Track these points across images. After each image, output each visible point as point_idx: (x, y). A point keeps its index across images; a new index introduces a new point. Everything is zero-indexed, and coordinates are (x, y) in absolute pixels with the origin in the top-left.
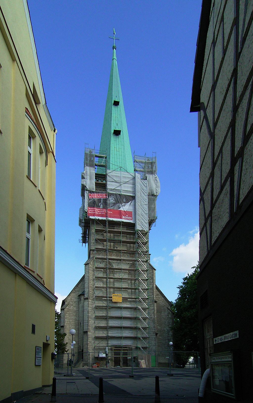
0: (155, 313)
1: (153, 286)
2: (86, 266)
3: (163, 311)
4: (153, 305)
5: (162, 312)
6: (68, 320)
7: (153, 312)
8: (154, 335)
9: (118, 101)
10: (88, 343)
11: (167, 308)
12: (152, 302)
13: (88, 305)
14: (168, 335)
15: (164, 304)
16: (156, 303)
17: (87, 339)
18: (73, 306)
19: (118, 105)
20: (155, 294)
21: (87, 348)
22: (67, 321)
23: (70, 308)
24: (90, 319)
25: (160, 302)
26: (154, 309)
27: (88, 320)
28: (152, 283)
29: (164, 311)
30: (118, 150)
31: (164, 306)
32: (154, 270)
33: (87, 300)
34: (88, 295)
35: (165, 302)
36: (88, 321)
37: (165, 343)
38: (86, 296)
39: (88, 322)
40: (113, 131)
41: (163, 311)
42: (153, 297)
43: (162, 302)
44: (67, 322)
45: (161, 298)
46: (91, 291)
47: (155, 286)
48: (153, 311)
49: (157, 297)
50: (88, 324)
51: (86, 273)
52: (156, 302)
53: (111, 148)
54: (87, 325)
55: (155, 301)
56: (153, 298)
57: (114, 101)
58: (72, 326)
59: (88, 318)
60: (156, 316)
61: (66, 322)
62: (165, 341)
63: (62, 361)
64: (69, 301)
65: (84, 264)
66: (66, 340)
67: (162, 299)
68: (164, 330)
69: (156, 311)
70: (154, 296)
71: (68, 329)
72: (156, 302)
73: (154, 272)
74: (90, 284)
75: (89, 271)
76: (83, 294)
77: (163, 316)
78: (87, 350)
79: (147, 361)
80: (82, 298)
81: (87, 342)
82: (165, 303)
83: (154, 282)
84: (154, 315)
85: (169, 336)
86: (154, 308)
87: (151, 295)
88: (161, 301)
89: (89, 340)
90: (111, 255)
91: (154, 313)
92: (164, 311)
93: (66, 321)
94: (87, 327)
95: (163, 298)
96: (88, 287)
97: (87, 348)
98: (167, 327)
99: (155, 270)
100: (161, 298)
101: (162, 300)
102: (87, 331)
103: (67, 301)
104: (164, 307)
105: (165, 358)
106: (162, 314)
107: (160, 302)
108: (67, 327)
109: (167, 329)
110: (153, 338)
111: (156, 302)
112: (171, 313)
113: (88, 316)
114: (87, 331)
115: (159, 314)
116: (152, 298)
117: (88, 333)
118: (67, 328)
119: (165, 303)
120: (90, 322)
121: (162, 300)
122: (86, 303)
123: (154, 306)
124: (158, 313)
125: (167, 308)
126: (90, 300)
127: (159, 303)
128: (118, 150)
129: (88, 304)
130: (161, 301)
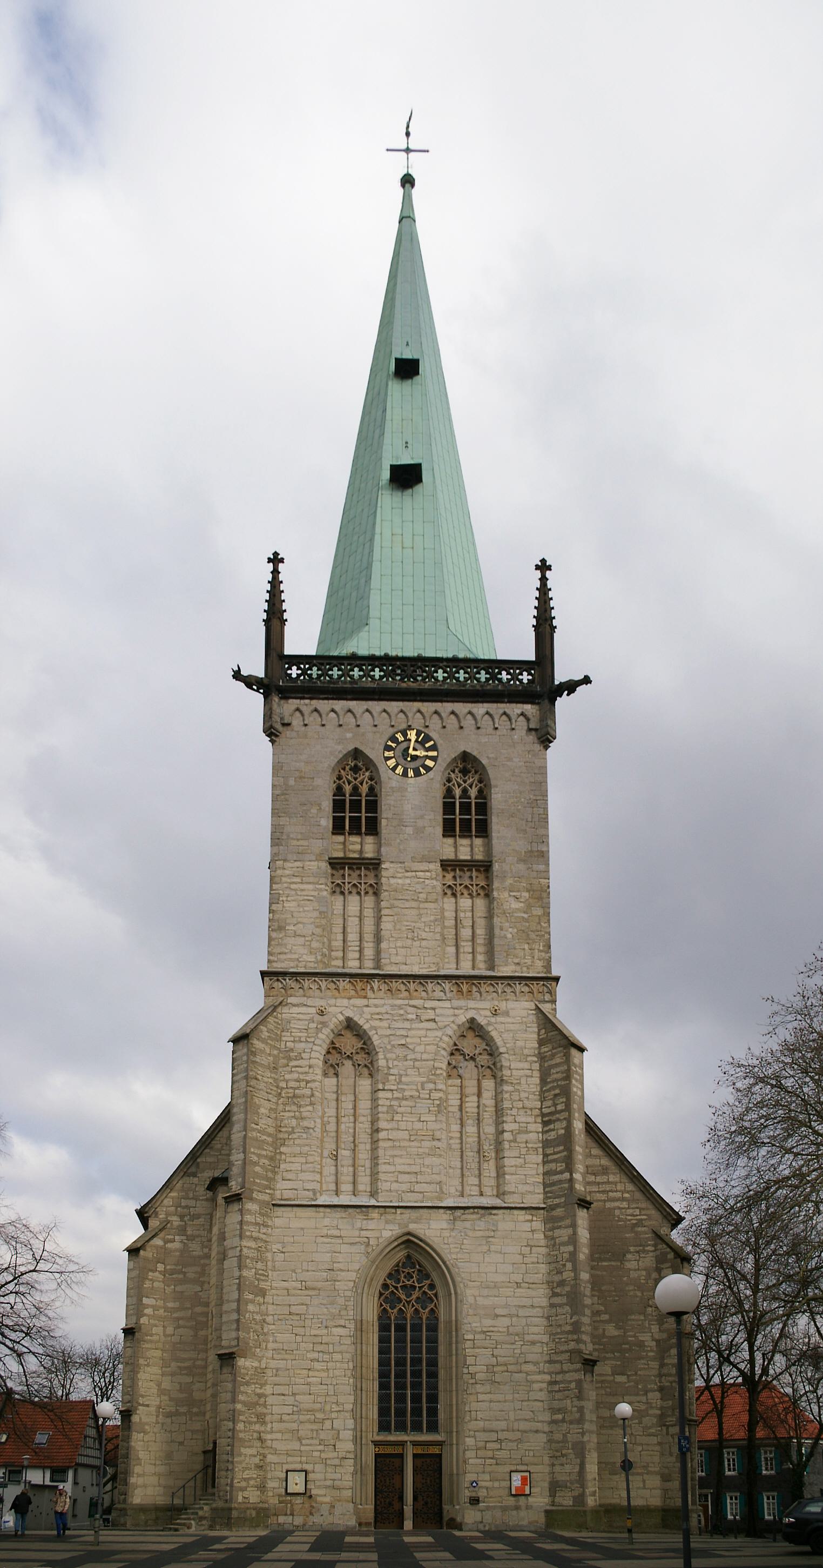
0: (582, 1257)
1: (569, 1129)
2: (236, 1048)
3: (632, 1249)
4: (568, 1222)
5: (629, 1256)
6: (160, 1303)
7: (570, 1253)
8: (576, 1371)
9: (415, 357)
10: (234, 1411)
11: (654, 1232)
12: (565, 1205)
13: (241, 1228)
14: (662, 1365)
15: (637, 1212)
16: (588, 1208)
17: (234, 1393)
18: (184, 1238)
19: (417, 373)
20: (580, 1167)
21: (230, 1434)
22: (152, 1306)
23: (169, 1245)
24: (251, 1297)
25: (619, 1208)
26: (573, 1240)
27: (238, 1301)
28: (562, 1111)
29: (638, 1249)
30: (408, 543)
31: (640, 1223)
32: (574, 1052)
33: (235, 1207)
34: (244, 1182)
35: (640, 1205)
36: (238, 1305)
37: (643, 1407)
38: (234, 1185)
39: (238, 1311)
40: (386, 474)
41: (632, 1249)
42: (571, 1180)
43: (625, 1204)
44: (155, 1308)
45: (619, 1187)
46: (256, 1164)
47: (578, 1125)
48: (571, 1248)
49: (603, 1183)
50: (238, 1321)
51: (236, 1078)
52: (585, 1204)
53: (377, 537)
54: (235, 1326)
55: (579, 1200)
56: (571, 1188)
57: (396, 359)
58: (179, 1328)
59: (239, 1289)
60: (585, 1276)
61: (147, 1311)
62: (644, 1399)
63: (123, 1496)
64: (167, 1214)
65: (230, 1037)
66: (143, 1396)
67: (628, 1192)
68: (641, 1345)
69: (586, 1250)
70: (577, 1176)
71: (160, 1345)
72: (585, 1204)
73: (576, 1061)
74: (254, 1130)
75: (247, 1070)
76: (222, 1181)
77: (633, 1275)
78: (233, 1446)
79: (570, 1508)
80: (222, 1194)
81: (231, 1406)
82: (641, 1209)
83: (575, 1106)
84: (575, 1269)
85: (665, 1371)
86: (575, 1233)
87: (561, 1172)
88: (623, 1199)
89: (241, 1397)
90: (362, 993)
91: (573, 1256)
92: (638, 1249)
93: (148, 1306)
94: (234, 1335)
95: (630, 1187)
96: (245, 1143)
97: (230, 1434)
98: (655, 1328)
99: (582, 1050)
100: (619, 1187)
101: (626, 1195)
102: (231, 1350)
103: (156, 1214)
104: (640, 1229)
105: (644, 1481)
106: (628, 1265)
107: (617, 1204)
108: (152, 1335)
109: (657, 1337)
110: (570, 1382)
111: (584, 1207)
112: (671, 1256)
113: (239, 1278)
114: (233, 1353)
115: (613, 1263)
116: (566, 1185)
117: (241, 1362)
118: (155, 1338)
119: (641, 1209)
120: (251, 1307)
121: (626, 1195)
122: (233, 1218)
123: (574, 1226)
124: (610, 1260)
125: (654, 1232)
126: (250, 1206)
127: (614, 1209)
128: (408, 543)
129: (241, 1223)
130: (623, 1199)
